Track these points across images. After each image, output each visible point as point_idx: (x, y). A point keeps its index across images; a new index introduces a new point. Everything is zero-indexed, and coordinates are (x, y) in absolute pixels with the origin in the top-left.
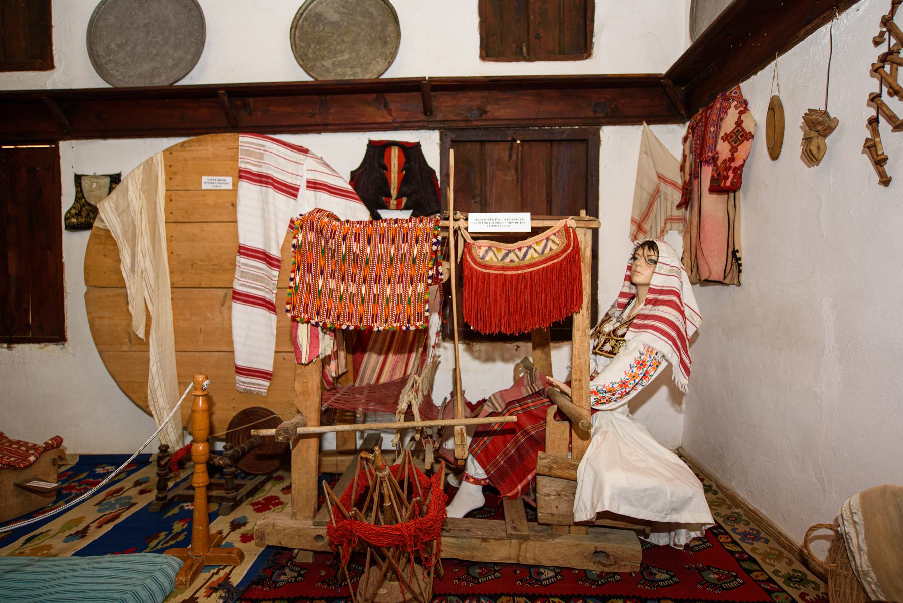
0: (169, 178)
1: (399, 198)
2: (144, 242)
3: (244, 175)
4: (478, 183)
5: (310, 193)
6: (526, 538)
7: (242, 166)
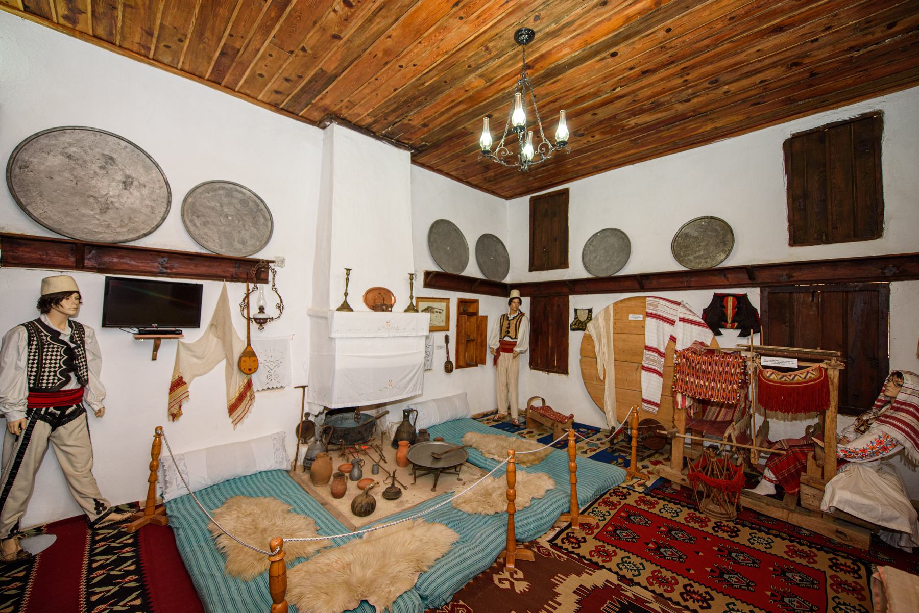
0: (615, 315)
1: (733, 321)
2: (604, 341)
3: (649, 315)
4: (788, 315)
5: (681, 323)
6: (793, 511)
7: (648, 310)
